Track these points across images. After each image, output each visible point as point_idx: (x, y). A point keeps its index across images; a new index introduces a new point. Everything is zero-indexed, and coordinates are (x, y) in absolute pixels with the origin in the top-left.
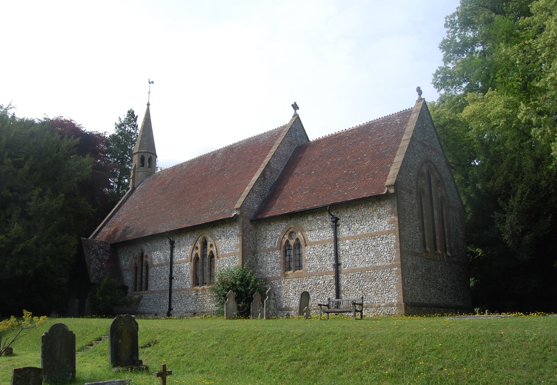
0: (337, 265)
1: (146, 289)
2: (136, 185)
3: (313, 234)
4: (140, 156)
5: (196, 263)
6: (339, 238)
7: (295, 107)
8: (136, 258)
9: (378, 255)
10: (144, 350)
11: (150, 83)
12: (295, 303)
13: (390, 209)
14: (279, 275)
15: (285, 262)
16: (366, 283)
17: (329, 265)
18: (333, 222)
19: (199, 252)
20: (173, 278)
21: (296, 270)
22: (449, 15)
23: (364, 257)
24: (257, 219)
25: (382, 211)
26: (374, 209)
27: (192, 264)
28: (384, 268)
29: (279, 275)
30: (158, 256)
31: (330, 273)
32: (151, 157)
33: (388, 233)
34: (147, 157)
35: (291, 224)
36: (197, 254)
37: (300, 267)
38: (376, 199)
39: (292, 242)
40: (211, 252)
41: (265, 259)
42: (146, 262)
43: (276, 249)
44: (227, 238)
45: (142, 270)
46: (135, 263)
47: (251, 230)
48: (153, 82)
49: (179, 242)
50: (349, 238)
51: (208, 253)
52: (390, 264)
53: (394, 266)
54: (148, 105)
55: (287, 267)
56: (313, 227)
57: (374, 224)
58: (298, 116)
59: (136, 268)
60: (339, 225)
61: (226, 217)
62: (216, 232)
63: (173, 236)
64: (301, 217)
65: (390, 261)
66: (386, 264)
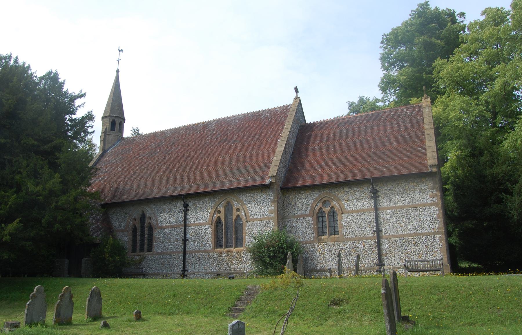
0: (378, 231)
1: (150, 249)
2: (106, 148)
3: (351, 203)
4: (111, 120)
5: (217, 226)
6: (380, 208)
9: (421, 224)
11: (120, 51)
12: (332, 264)
13: (432, 185)
14: (312, 239)
15: (318, 228)
16: (409, 247)
17: (369, 231)
18: (185, 207)
19: (222, 216)
20: (188, 240)
21: (331, 235)
22: (386, 33)
23: (410, 226)
24: (288, 186)
25: (423, 186)
26: (415, 184)
27: (213, 227)
28: (427, 235)
30: (167, 218)
31: (370, 238)
32: (121, 122)
33: (431, 205)
34: (118, 122)
35: (326, 193)
36: (219, 218)
37: (335, 233)
38: (264, 188)
39: (326, 210)
40: (238, 216)
41: (294, 224)
42: (150, 223)
43: (307, 216)
44: (258, 203)
45: (143, 232)
46: (134, 225)
48: (122, 51)
49: (194, 204)
50: (390, 208)
52: (433, 231)
53: (438, 233)
54: (118, 71)
55: (320, 232)
56: (350, 197)
57: (416, 197)
58: (300, 100)
59: (135, 230)
60: (378, 197)
61: (248, 185)
62: (243, 197)
63: (186, 199)
64: (336, 187)
65: (434, 229)
66: (430, 231)
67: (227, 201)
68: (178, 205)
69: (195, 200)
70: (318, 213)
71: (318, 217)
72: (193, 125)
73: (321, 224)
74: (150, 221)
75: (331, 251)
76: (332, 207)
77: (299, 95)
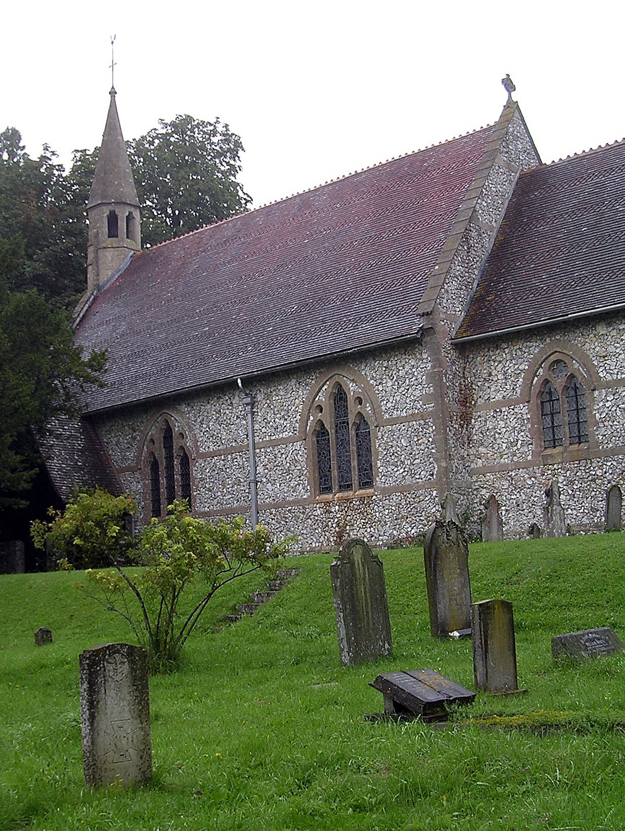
7: (508, 84)
8: (152, 441)
10: (60, 632)
14: (530, 458)
29: (530, 458)
37: (580, 438)
41: (490, 425)
42: (182, 448)
45: (170, 468)
46: (152, 454)
47: (453, 363)
49: (268, 396)
51: (351, 418)
54: (113, 93)
56: (611, 349)
59: (155, 466)
67: (333, 381)
68: (236, 401)
69: (268, 386)
70: (541, 393)
71: (542, 403)
72: (469, 136)
73: (548, 419)
74: (181, 442)
75: (572, 482)
76: (572, 376)
77: (515, 96)
